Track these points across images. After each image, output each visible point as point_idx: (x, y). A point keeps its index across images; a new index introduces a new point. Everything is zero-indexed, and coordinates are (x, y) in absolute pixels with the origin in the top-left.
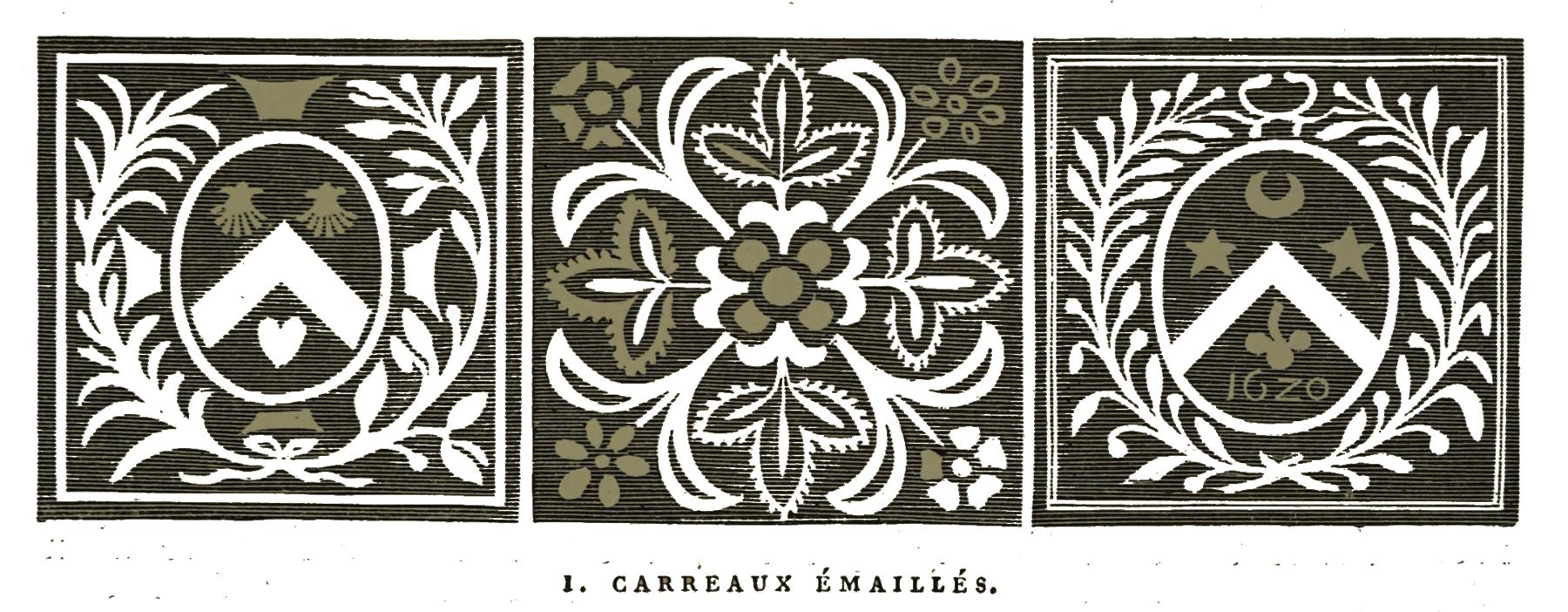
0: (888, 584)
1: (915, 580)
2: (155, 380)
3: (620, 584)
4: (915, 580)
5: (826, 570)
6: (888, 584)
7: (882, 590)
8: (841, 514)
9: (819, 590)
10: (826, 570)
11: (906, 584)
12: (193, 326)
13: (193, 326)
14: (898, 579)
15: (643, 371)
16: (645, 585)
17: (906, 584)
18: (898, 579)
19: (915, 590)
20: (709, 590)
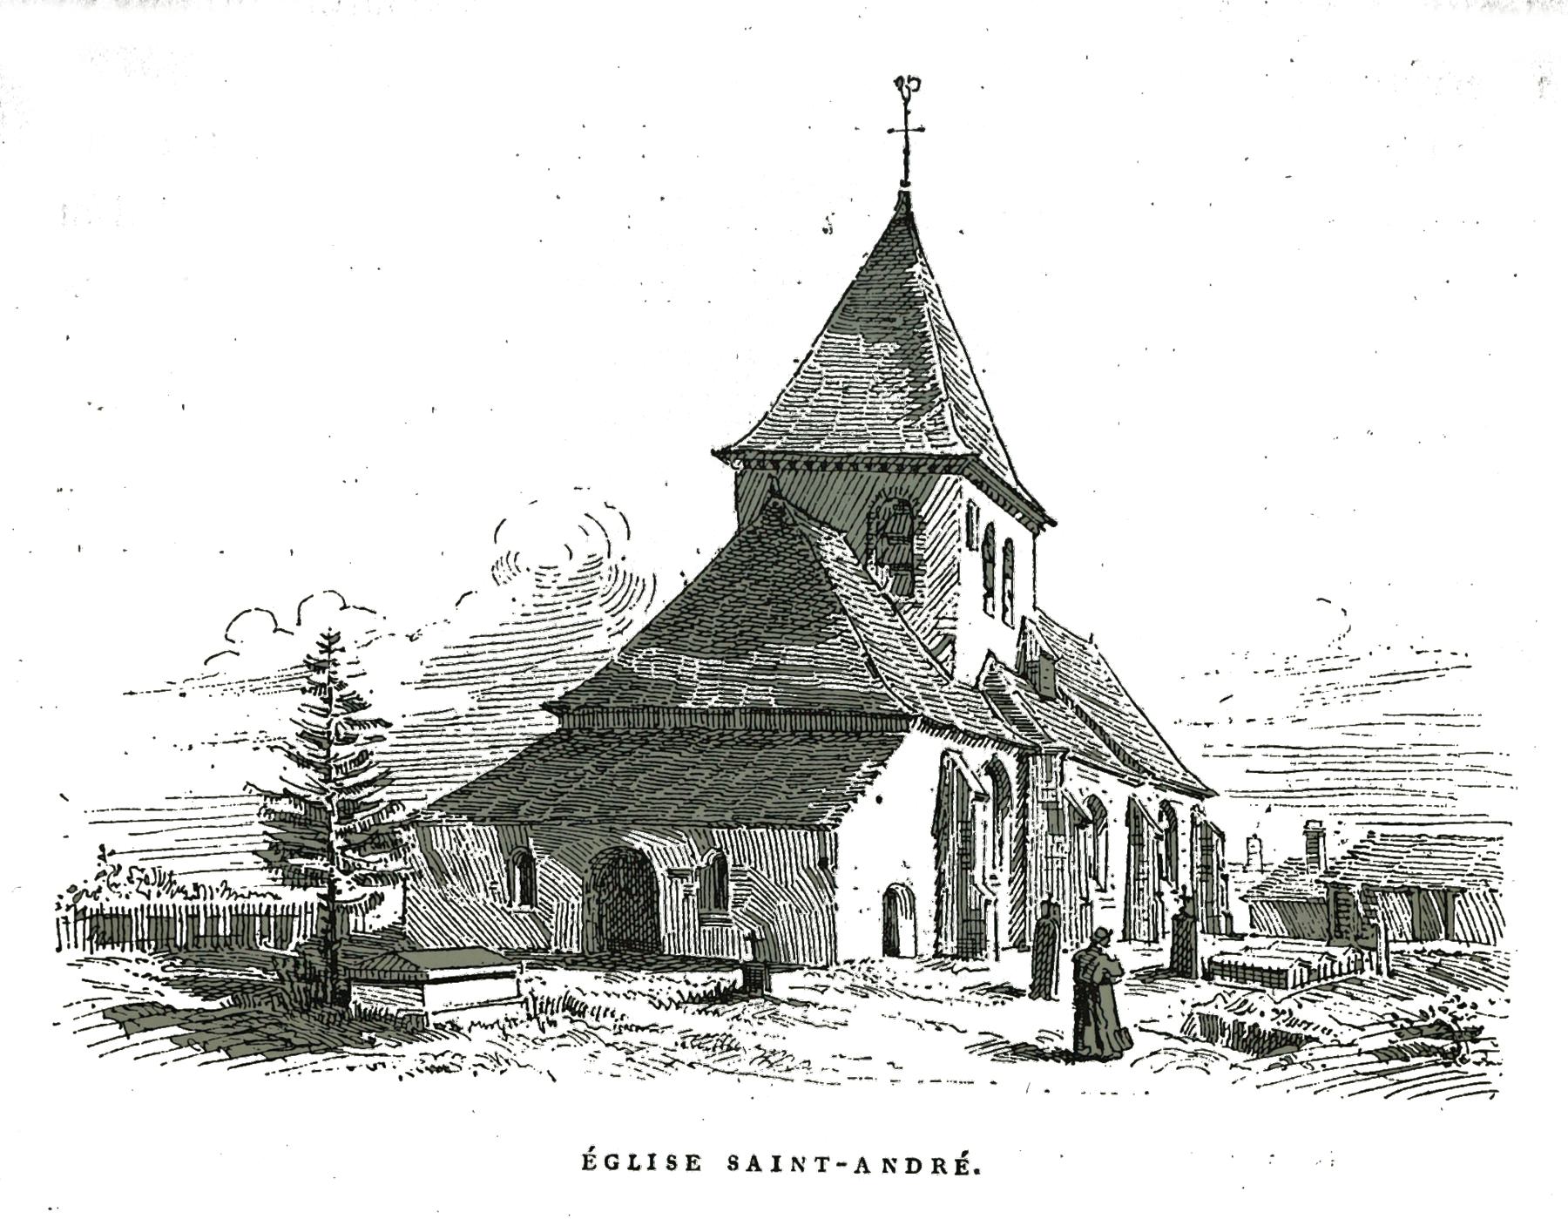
0: (766, 1163)
1: (633, 1157)
2: (299, 717)
3: (612, 1161)
4: (633, 1157)
5: (592, 1148)
6: (766, 1163)
7: (758, 1169)
8: (642, 646)
9: (585, 1168)
10: (592, 1148)
11: (661, 1162)
12: (906, 163)
13: (906, 163)
14: (777, 1158)
15: (1294, 972)
16: (756, 1165)
17: (661, 1162)
18: (777, 1158)
19: (631, 1167)
20: (689, 1168)
